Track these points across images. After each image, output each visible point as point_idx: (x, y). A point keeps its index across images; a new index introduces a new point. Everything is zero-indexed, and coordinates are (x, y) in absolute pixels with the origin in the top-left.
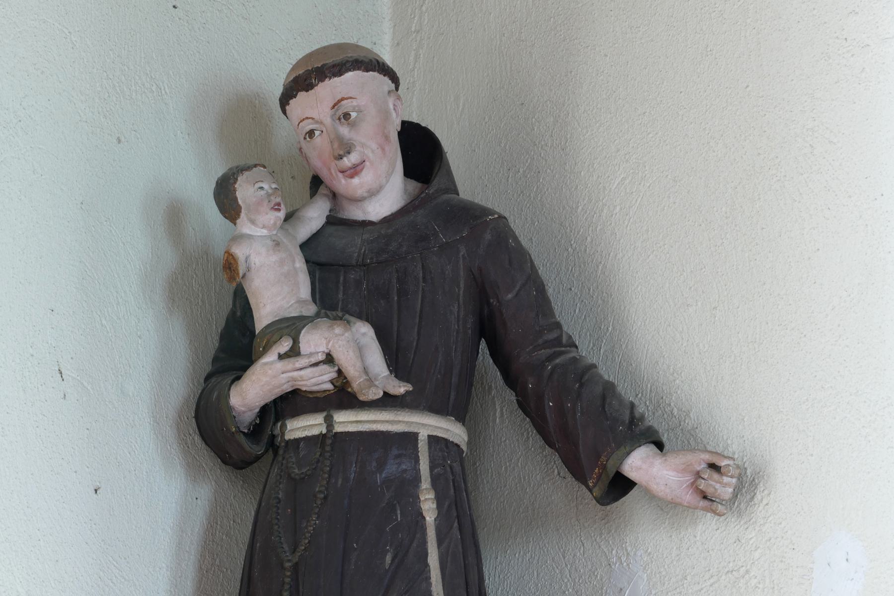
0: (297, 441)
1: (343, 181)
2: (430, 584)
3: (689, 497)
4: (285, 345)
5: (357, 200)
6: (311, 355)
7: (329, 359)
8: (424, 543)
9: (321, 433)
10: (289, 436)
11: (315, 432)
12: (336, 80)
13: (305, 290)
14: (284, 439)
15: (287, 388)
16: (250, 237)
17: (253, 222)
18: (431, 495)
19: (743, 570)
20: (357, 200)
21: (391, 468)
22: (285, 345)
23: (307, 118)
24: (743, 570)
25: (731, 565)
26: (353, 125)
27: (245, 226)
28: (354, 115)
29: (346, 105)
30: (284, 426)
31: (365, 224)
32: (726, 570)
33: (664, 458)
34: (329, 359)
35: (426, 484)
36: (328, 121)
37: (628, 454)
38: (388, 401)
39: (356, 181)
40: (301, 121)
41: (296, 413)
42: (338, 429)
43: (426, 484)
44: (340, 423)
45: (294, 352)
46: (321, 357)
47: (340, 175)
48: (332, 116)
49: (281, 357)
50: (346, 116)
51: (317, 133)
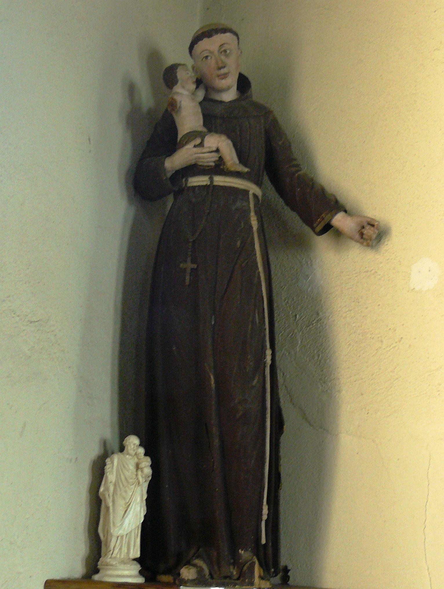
0: (194, 187)
1: (217, 81)
2: (256, 257)
3: (357, 236)
4: (198, 141)
5: (220, 91)
6: (209, 147)
7: (217, 151)
8: (253, 239)
9: (207, 185)
10: (189, 185)
11: (205, 184)
12: (222, 35)
13: (201, 122)
14: (187, 186)
15: (193, 162)
16: (181, 94)
17: (183, 87)
18: (255, 218)
19: (373, 271)
20: (220, 91)
21: (239, 204)
22: (198, 141)
23: (231, 31)
24: (373, 271)
25: (367, 268)
26: (227, 56)
27: (177, 88)
28: (228, 52)
29: (226, 47)
30: (187, 180)
31: (221, 102)
32: (364, 271)
33: (352, 218)
34: (217, 151)
35: (252, 214)
36: (216, 53)
37: (336, 214)
38: (238, 174)
39: (223, 81)
40: (203, 52)
41: (195, 175)
42: (215, 183)
43: (252, 214)
44: (217, 181)
45: (201, 145)
46: (214, 149)
47: (217, 78)
48: (219, 51)
49: (195, 146)
50: (225, 51)
51: (209, 58)
